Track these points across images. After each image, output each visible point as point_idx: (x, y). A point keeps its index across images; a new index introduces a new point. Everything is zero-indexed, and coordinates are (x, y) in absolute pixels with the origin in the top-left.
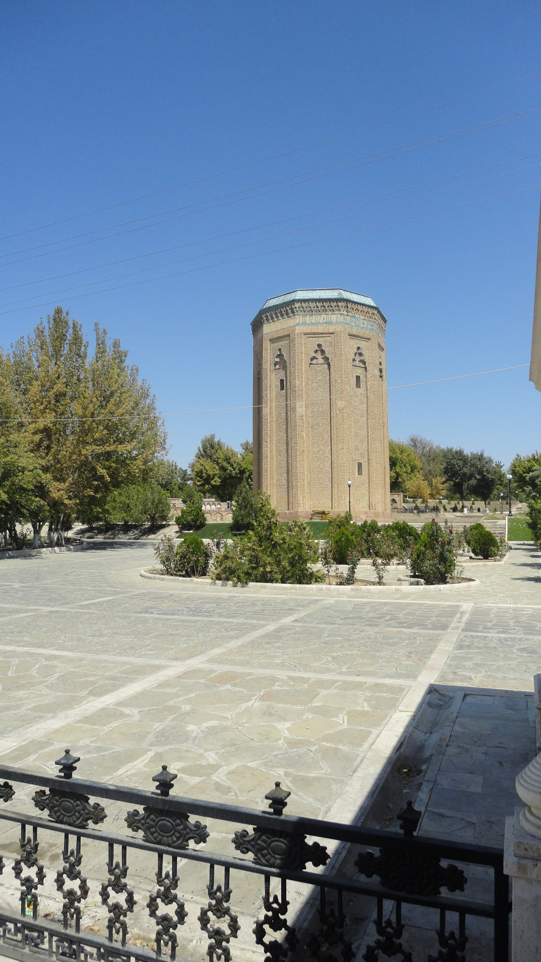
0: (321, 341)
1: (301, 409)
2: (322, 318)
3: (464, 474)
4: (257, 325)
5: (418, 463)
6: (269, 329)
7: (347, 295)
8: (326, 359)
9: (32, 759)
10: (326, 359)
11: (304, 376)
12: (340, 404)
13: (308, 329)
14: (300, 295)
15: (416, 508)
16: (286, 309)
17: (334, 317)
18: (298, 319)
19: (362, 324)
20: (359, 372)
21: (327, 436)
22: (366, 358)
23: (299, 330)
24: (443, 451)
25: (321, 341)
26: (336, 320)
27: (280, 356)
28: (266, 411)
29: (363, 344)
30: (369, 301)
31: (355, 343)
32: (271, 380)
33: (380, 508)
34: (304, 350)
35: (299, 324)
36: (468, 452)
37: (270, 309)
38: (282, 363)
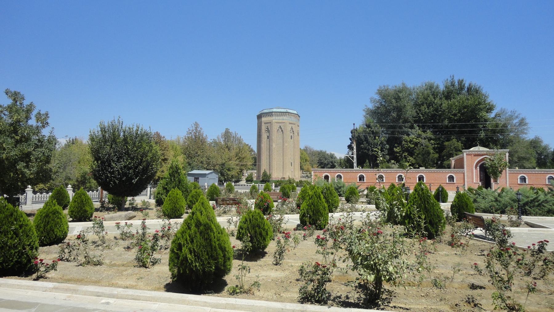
0: (280, 125)
1: (274, 146)
2: (281, 118)
3: (325, 164)
4: (259, 117)
5: (308, 159)
6: (264, 119)
7: (289, 111)
8: (282, 130)
9: (103, 301)
10: (282, 130)
11: (276, 136)
12: (286, 144)
13: (277, 121)
14: (275, 110)
15: (307, 176)
16: (270, 114)
17: (285, 118)
18: (274, 118)
19: (293, 119)
20: (292, 134)
21: (282, 154)
22: (294, 130)
23: (274, 121)
24: (318, 151)
25: (280, 125)
26: (285, 118)
27: (268, 128)
28: (263, 145)
29: (293, 126)
30: (295, 112)
31: (291, 126)
32: (264, 135)
33: (297, 177)
34: (275, 127)
35: (274, 119)
36: (328, 152)
37: (264, 113)
38: (268, 131)
